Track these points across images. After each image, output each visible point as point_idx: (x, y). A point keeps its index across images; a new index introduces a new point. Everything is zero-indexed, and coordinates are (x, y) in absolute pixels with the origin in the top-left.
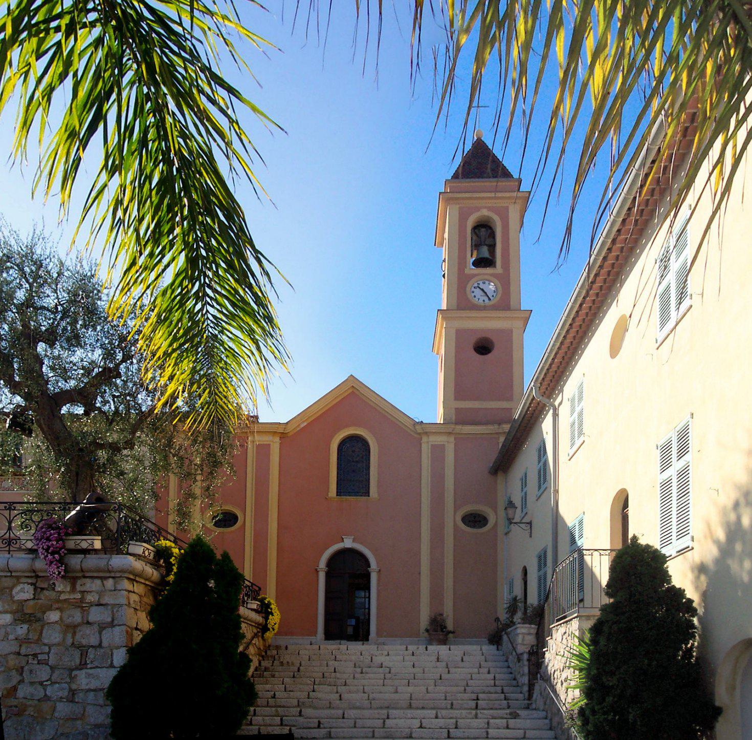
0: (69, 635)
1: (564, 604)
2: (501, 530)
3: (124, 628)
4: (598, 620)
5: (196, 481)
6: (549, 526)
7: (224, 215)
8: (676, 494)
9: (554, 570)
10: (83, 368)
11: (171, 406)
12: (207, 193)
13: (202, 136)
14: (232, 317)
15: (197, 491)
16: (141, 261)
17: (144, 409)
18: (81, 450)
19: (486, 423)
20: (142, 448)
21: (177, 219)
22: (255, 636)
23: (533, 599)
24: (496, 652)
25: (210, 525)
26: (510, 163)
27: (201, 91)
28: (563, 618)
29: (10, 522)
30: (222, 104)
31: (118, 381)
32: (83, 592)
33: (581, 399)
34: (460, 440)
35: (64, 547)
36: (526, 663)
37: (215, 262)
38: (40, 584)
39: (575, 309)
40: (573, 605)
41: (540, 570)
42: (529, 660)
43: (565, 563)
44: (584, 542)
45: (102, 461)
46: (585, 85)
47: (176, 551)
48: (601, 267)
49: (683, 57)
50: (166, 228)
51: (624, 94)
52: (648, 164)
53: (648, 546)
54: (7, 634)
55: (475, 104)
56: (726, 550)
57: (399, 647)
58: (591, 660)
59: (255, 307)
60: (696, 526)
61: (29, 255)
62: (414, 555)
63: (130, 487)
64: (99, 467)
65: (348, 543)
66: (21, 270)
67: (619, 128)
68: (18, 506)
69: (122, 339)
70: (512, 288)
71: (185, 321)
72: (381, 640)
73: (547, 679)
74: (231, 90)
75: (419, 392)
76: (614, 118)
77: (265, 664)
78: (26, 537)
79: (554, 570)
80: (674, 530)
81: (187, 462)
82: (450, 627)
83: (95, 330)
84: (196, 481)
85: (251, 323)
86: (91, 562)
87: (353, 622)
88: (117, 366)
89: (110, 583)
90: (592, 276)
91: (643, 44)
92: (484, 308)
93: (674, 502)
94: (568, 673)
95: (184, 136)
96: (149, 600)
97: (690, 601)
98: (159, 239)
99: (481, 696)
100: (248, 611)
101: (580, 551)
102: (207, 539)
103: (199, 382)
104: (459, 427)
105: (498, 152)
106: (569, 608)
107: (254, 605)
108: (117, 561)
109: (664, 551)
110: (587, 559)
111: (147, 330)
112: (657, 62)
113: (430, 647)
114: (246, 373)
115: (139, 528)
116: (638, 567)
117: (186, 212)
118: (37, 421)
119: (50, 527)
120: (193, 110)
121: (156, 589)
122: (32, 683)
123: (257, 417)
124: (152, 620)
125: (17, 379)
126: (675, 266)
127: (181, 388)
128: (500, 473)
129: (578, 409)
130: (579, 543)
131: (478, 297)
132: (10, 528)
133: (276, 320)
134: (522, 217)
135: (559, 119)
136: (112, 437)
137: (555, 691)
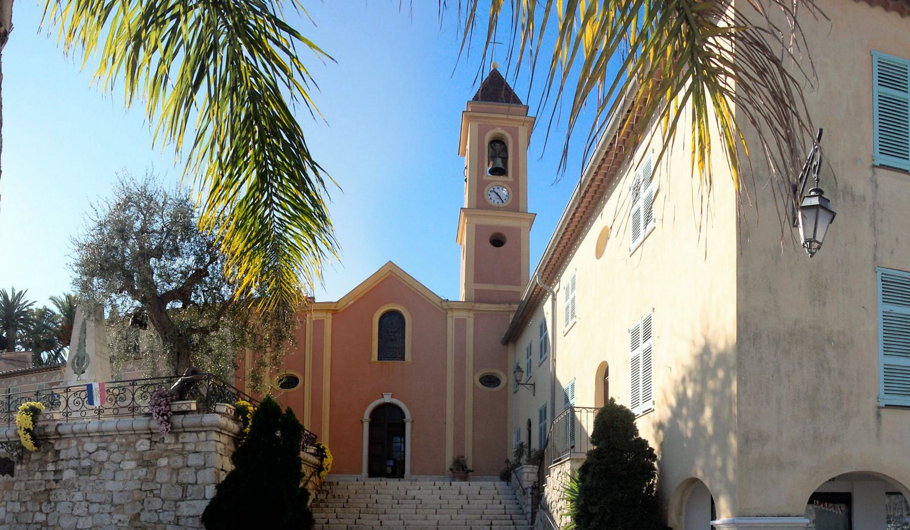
0: (175, 476)
1: (559, 448)
2: (511, 389)
3: (213, 469)
4: (586, 462)
5: (266, 352)
6: (549, 388)
7: (287, 136)
8: (642, 367)
9: (552, 423)
10: (181, 272)
11: (246, 294)
12: (273, 119)
13: (269, 73)
14: (293, 218)
15: (267, 360)
16: (223, 182)
17: (226, 298)
18: (181, 335)
19: (499, 303)
20: (225, 329)
21: (250, 143)
22: (313, 474)
23: (535, 445)
24: (507, 487)
25: (277, 387)
26: (520, 91)
27: (268, 36)
28: (558, 461)
29: (133, 395)
30: (285, 44)
31: (207, 279)
32: (183, 443)
33: (573, 288)
34: (479, 315)
35: (170, 410)
36: (530, 496)
37: (280, 174)
38: (154, 439)
39: (570, 217)
40: (567, 450)
41: (541, 422)
42: (532, 493)
43: (561, 417)
44: (575, 402)
45: (196, 342)
46: (579, 39)
47: (251, 408)
48: (590, 186)
49: (651, 36)
50: (241, 153)
51: (608, 53)
52: (625, 112)
53: (621, 406)
54: (133, 476)
55: (492, 40)
56: (676, 413)
57: (428, 483)
58: (580, 493)
59: (312, 208)
60: (656, 394)
61: (143, 193)
62: (441, 411)
63: (216, 361)
64: (194, 347)
65: (387, 399)
66: (139, 206)
67: (603, 79)
68: (139, 383)
69: (210, 245)
70: (520, 194)
71: (256, 225)
72: (414, 477)
73: (546, 508)
74: (292, 32)
75: (445, 275)
76: (600, 70)
77: (321, 496)
78: (145, 405)
79: (552, 423)
80: (641, 395)
81: (259, 337)
82: (470, 467)
83: (189, 241)
84: (266, 352)
85: (308, 222)
86: (190, 420)
87: (391, 463)
88: (206, 267)
89: (202, 436)
90: (583, 192)
91: (622, 17)
92: (498, 209)
93: (641, 374)
94: (562, 504)
95: (255, 75)
96: (232, 448)
97: (652, 450)
98: (236, 162)
99: (494, 522)
100: (307, 455)
101: (572, 408)
102: (275, 398)
103: (267, 273)
104: (478, 305)
105: (510, 82)
106: (564, 452)
107: (312, 450)
108: (208, 419)
109: (633, 411)
110: (577, 414)
111: (227, 236)
112: (632, 34)
113: (453, 483)
114: (305, 263)
115: (223, 392)
116: (615, 422)
117: (257, 137)
118: (151, 317)
119: (161, 396)
120: (262, 53)
121: (236, 438)
122: (150, 511)
123: (313, 298)
124: (234, 462)
125: (136, 288)
126: (644, 195)
127: (253, 279)
128: (510, 344)
129: (571, 297)
130: (571, 402)
131: (494, 200)
132: (133, 399)
133: (329, 218)
134: (529, 137)
135: (559, 62)
136: (203, 323)
137: (552, 518)
